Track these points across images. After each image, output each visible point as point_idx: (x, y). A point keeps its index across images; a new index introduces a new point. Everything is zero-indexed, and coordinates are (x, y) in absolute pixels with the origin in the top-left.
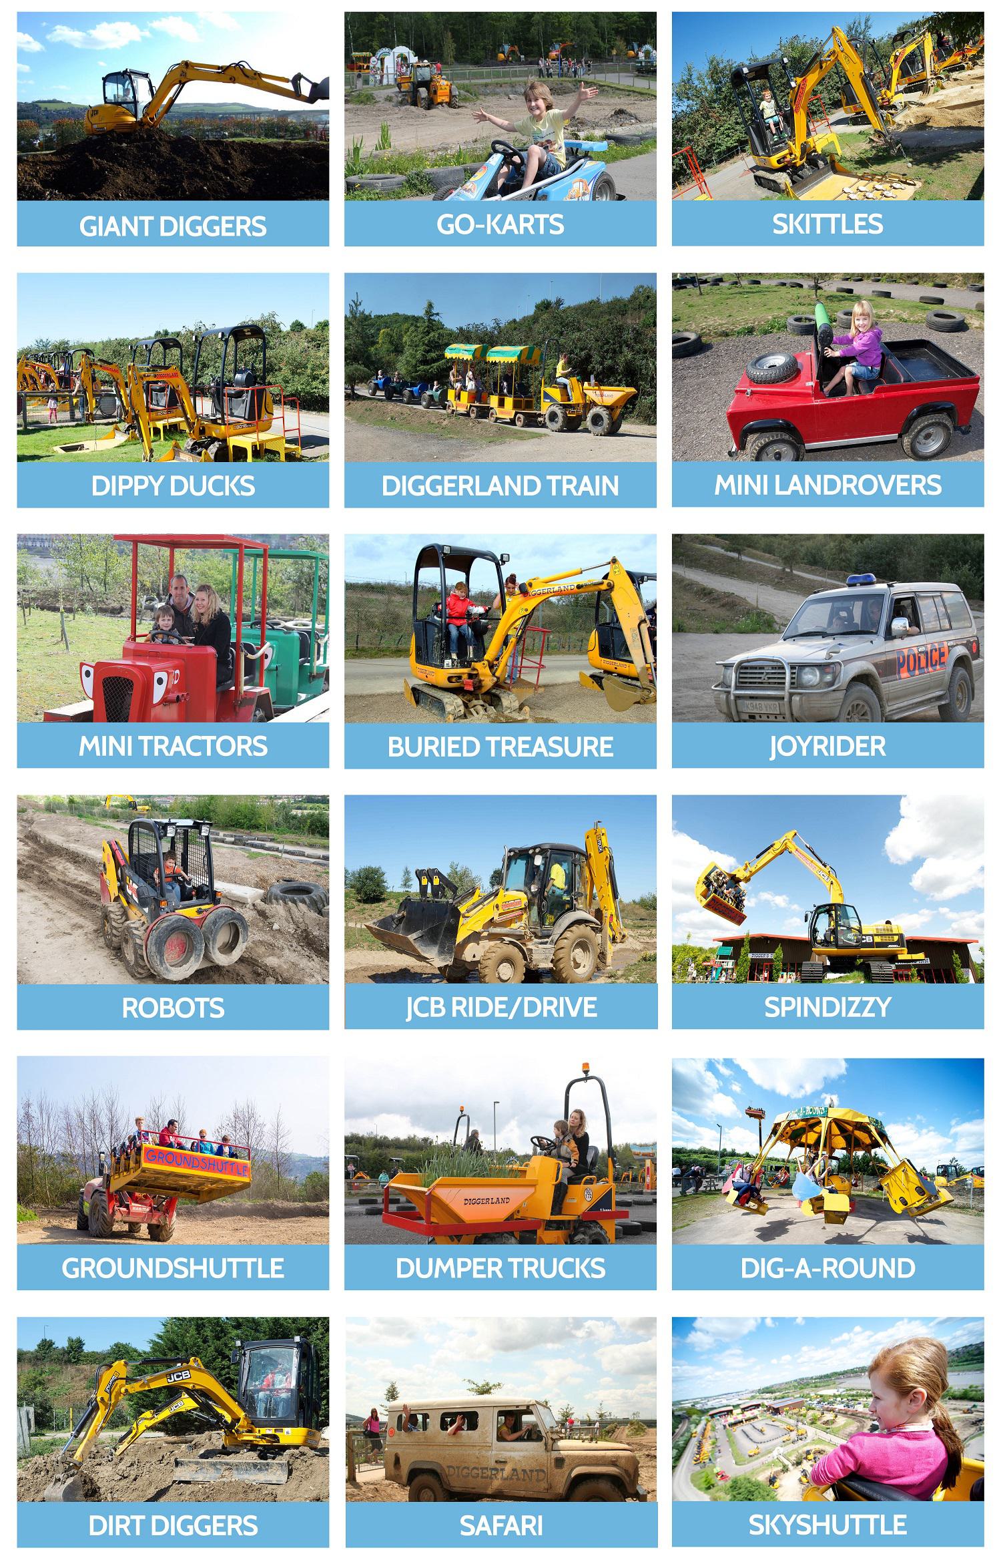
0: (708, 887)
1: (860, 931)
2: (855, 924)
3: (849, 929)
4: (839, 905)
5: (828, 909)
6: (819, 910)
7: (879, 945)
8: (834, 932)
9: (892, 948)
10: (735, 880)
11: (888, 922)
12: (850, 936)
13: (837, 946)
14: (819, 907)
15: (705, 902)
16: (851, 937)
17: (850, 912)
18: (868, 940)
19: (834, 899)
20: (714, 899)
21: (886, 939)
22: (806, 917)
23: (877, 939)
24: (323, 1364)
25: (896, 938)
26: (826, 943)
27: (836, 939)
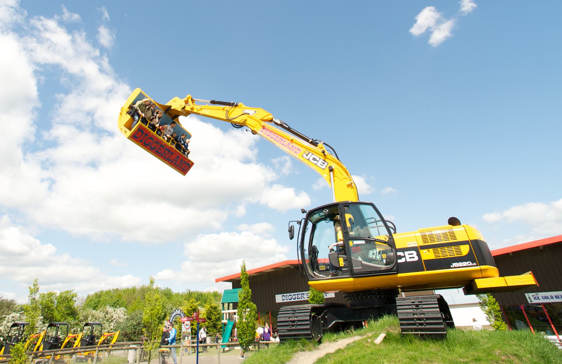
0: (133, 116)
1: (391, 243)
2: (379, 233)
3: (371, 242)
4: (347, 204)
5: (333, 212)
6: (313, 216)
7: (431, 264)
8: (343, 250)
9: (458, 268)
10: (172, 115)
11: (453, 221)
12: (374, 254)
13: (353, 274)
14: (311, 213)
15: (129, 133)
16: (376, 257)
17: (367, 212)
18: (410, 257)
19: (340, 195)
20: (140, 129)
21: (448, 253)
22: (291, 230)
23: (428, 255)
24: (517, 324)
25: (465, 250)
26: (334, 270)
27: (348, 261)
